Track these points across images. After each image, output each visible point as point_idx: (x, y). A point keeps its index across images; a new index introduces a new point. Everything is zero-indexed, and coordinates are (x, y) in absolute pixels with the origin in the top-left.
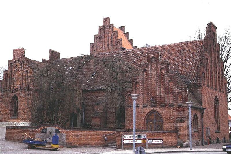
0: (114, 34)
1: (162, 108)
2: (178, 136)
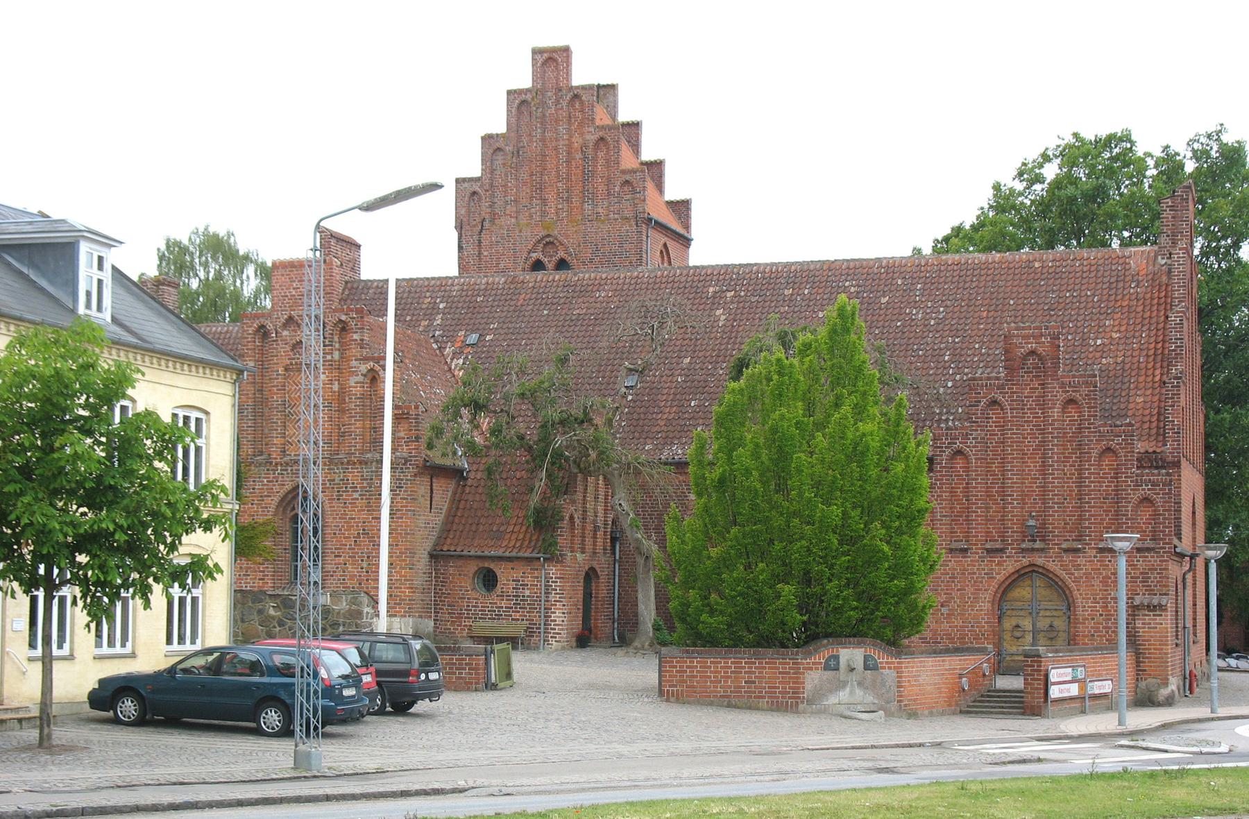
0: (602, 139)
1: (1067, 558)
2: (1139, 666)
